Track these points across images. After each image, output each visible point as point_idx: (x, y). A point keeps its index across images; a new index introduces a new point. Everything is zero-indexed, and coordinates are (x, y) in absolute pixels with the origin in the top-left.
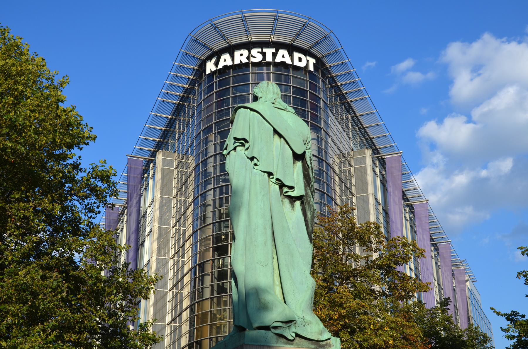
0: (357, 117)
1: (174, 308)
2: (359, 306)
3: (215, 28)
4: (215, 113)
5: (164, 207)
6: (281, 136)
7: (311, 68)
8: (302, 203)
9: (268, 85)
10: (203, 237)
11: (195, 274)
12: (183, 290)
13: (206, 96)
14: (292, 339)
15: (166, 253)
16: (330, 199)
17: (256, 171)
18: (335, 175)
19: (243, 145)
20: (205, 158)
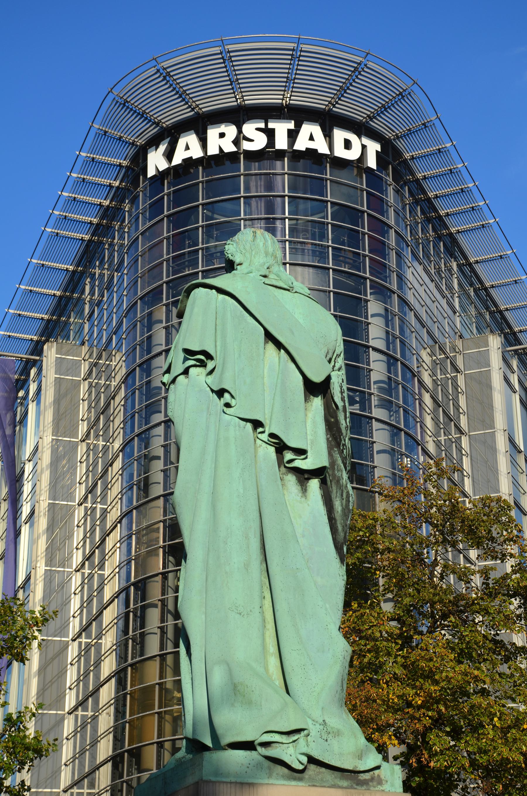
0: (470, 265)
1: (82, 678)
2: (467, 679)
3: (165, 78)
4: (168, 260)
5: (62, 457)
6: (279, 345)
7: (372, 162)
8: (323, 483)
9: (255, 236)
10: (145, 524)
11: (127, 605)
12: (101, 638)
13: (148, 224)
14: (301, 767)
15: (65, 562)
16: (411, 441)
17: (229, 418)
18: (423, 391)
19: (203, 364)
20: (146, 357)
